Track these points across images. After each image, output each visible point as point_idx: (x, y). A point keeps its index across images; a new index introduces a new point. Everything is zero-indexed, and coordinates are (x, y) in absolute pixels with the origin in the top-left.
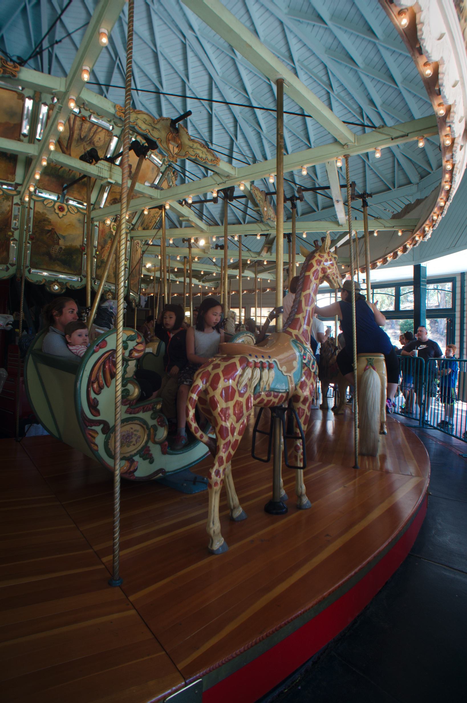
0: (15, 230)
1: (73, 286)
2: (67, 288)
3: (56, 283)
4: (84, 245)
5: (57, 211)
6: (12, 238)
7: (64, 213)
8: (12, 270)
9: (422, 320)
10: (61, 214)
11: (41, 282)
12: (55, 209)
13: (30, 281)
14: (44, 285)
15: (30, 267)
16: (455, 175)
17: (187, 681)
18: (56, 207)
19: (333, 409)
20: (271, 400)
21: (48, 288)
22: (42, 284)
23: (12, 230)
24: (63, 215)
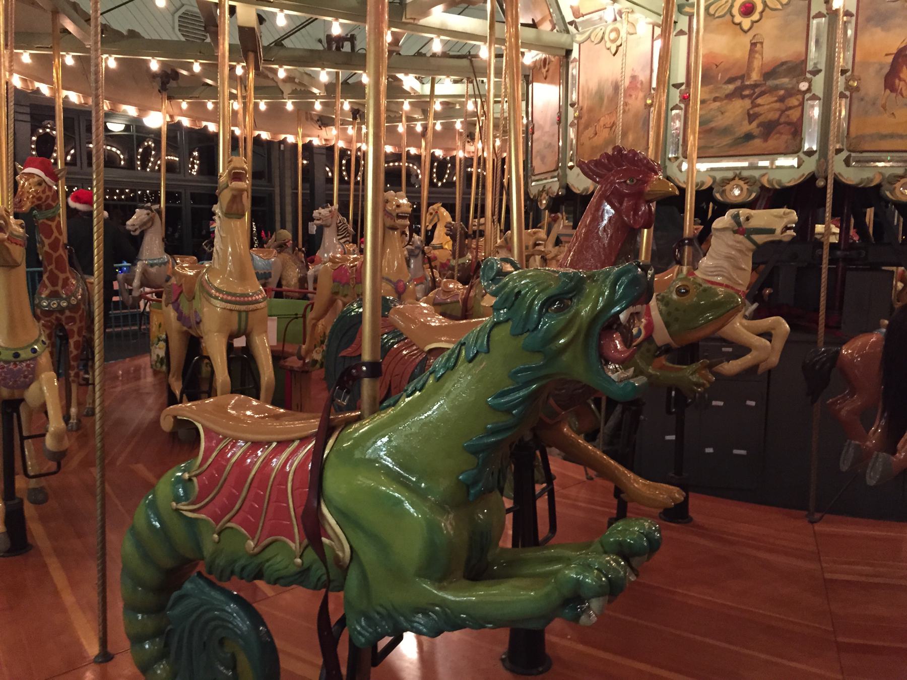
0: (815, 76)
1: (779, 182)
2: (763, 187)
3: (737, 181)
4: (653, 92)
5: (738, 19)
6: (807, 96)
7: (756, 17)
8: (811, 165)
9: (372, 83)
10: (746, 23)
11: (872, 180)
12: (733, 16)
13: (844, 180)
14: (879, 186)
15: (801, 154)
16: (99, 603)
17: (90, 357)
18: (735, 11)
19: (403, 502)
20: (17, 225)
21: (888, 193)
22: (872, 185)
23: (808, 76)
24: (753, 22)
